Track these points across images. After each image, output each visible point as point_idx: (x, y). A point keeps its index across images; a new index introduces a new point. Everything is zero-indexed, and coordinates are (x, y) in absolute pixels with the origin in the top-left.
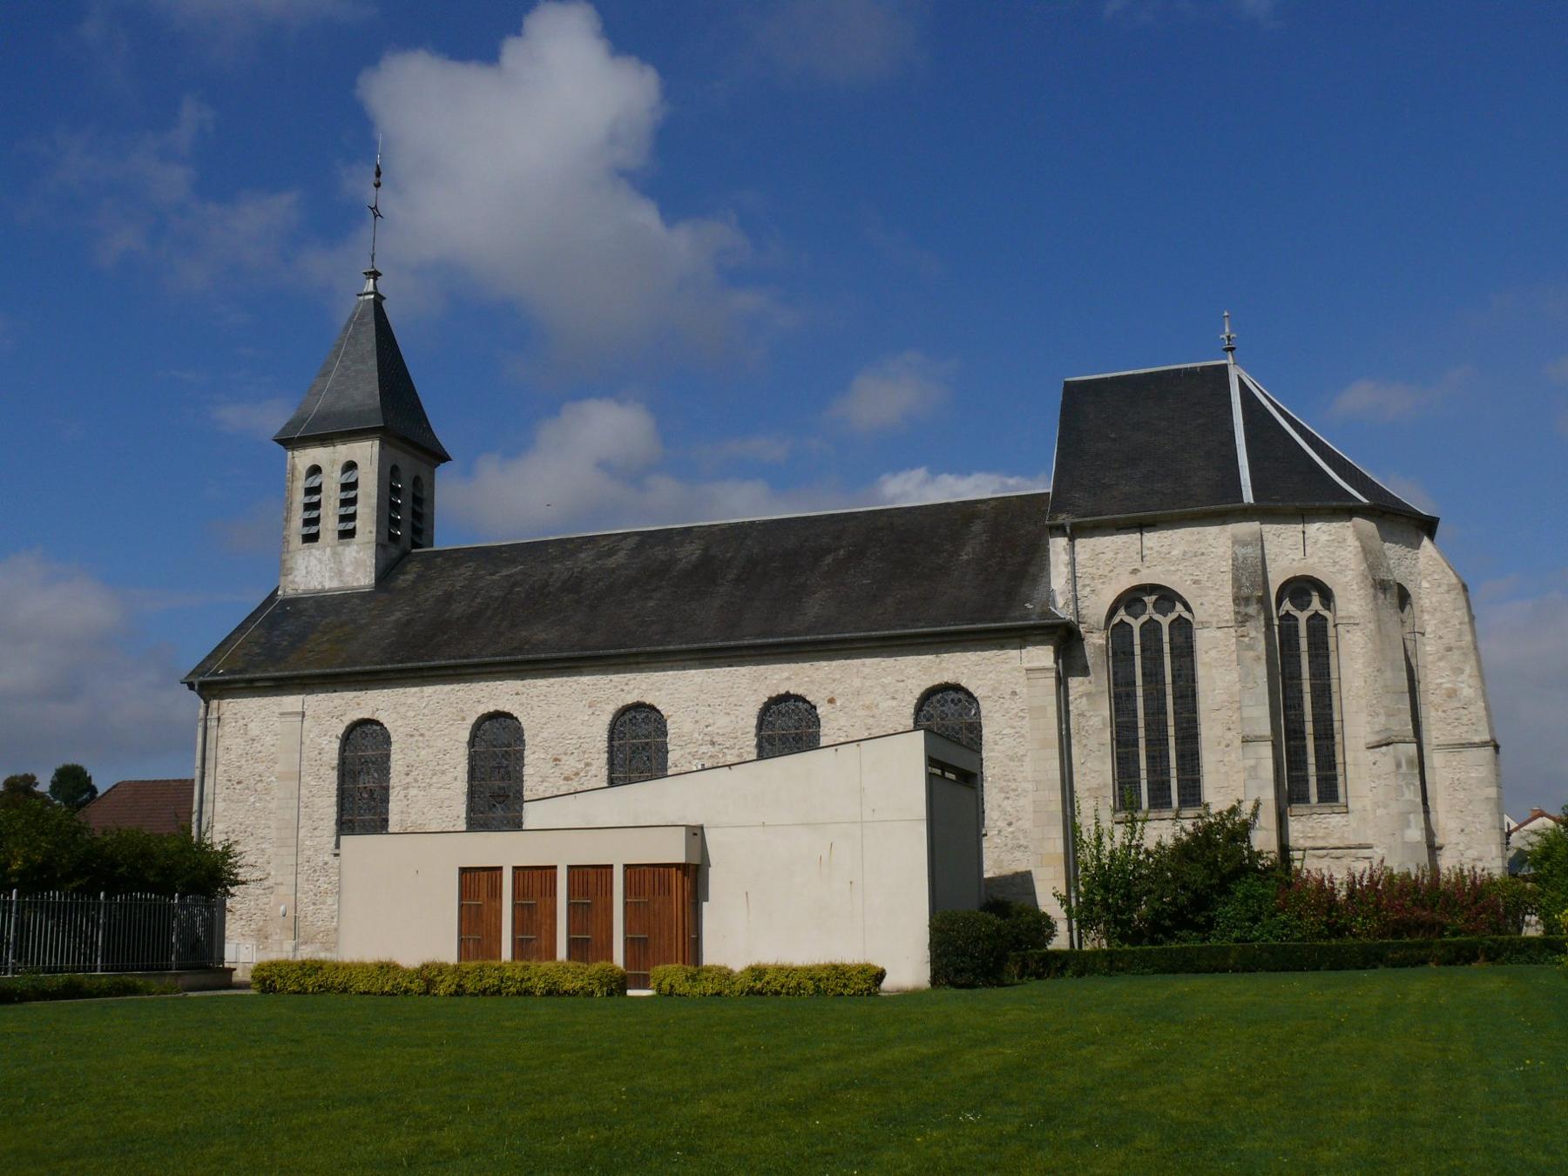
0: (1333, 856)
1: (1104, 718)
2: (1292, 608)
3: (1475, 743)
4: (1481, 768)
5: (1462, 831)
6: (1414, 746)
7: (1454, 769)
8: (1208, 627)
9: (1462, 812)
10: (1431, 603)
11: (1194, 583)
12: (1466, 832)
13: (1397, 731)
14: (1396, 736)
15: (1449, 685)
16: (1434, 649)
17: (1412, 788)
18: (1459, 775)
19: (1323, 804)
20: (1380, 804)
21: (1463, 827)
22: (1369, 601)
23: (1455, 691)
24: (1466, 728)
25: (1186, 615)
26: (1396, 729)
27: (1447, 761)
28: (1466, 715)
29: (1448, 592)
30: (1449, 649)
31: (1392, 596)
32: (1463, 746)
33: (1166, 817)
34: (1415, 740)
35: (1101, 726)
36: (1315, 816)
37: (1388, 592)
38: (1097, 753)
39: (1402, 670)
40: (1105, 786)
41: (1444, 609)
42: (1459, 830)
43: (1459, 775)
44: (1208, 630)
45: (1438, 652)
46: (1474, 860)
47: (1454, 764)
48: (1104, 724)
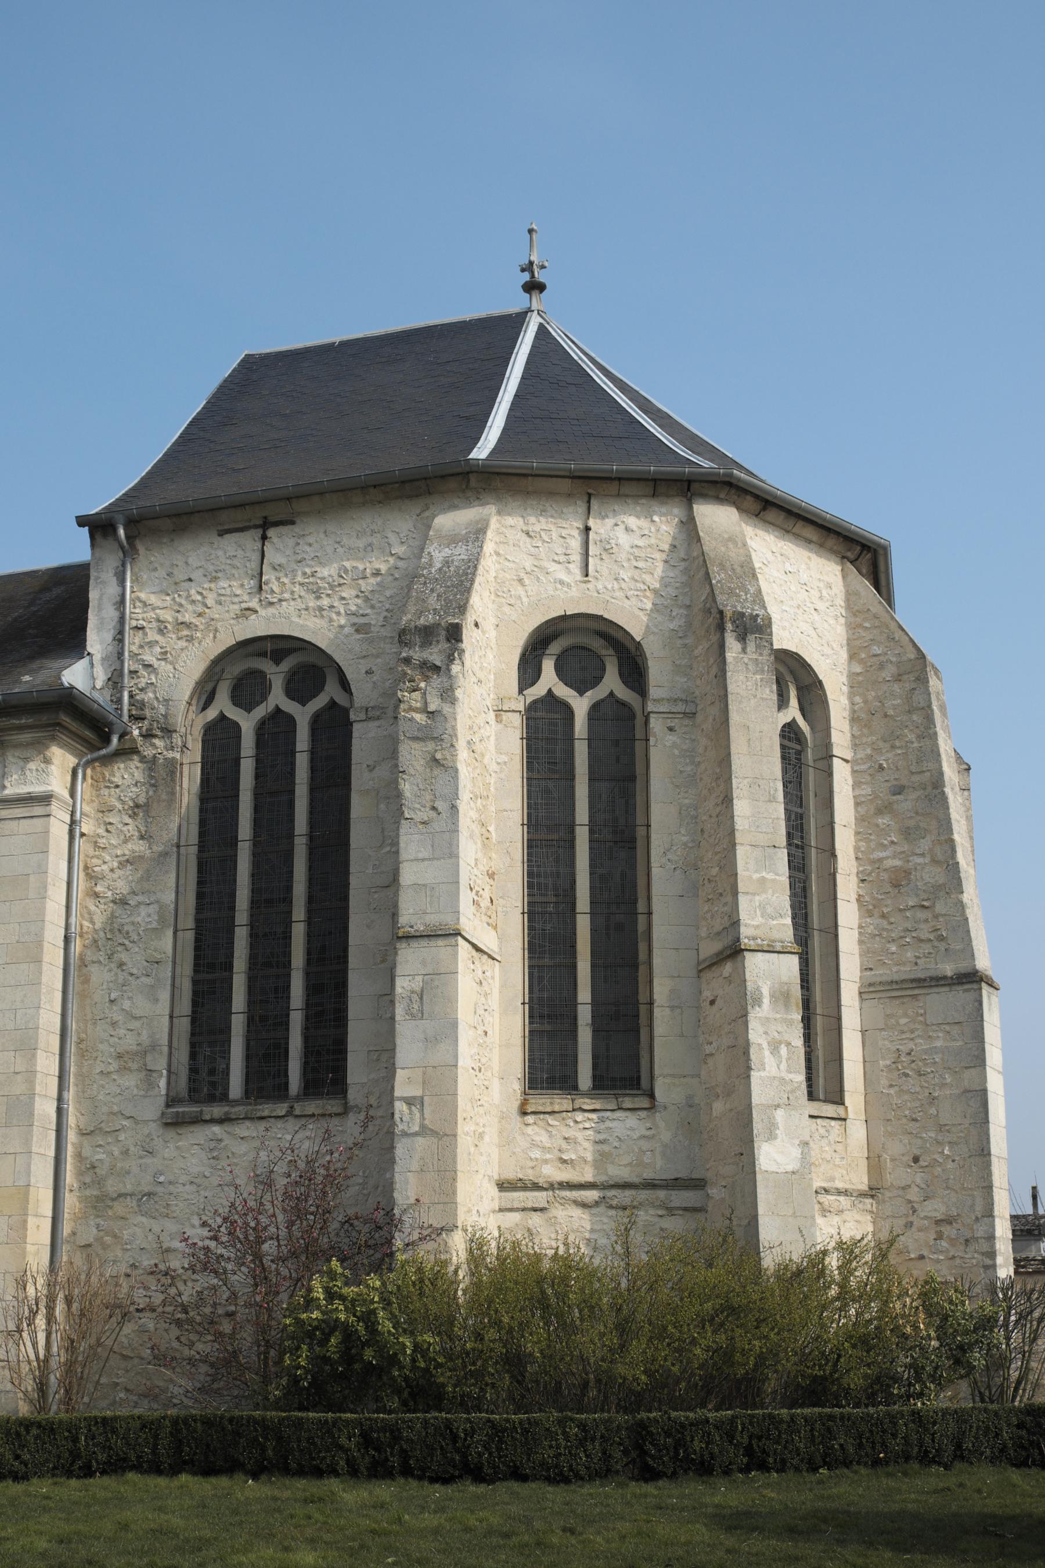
0: (614, 1203)
1: (162, 907)
2: (570, 701)
3: (945, 978)
4: (955, 1030)
5: (916, 1160)
6: (794, 961)
7: (903, 1032)
8: (378, 718)
9: (915, 1120)
10: (865, 702)
11: (357, 631)
12: (922, 1163)
13: (757, 927)
14: (754, 939)
15: (897, 863)
16: (869, 791)
17: (783, 1050)
18: (911, 1045)
19: (597, 1092)
20: (719, 1090)
21: (917, 1152)
22: (712, 661)
23: (907, 873)
24: (927, 948)
25: (341, 699)
26: (755, 923)
27: (889, 1016)
28: (926, 921)
29: (898, 678)
30: (899, 790)
31: (758, 647)
32: (920, 983)
33: (266, 1113)
34: (796, 948)
35: (154, 925)
36: (579, 1116)
37: (751, 637)
38: (144, 979)
39: (772, 800)
40: (154, 1047)
41: (891, 712)
42: (908, 1159)
43: (911, 1045)
44: (377, 723)
45: (877, 797)
46: (938, 1222)
47: (903, 1021)
48: (162, 920)
